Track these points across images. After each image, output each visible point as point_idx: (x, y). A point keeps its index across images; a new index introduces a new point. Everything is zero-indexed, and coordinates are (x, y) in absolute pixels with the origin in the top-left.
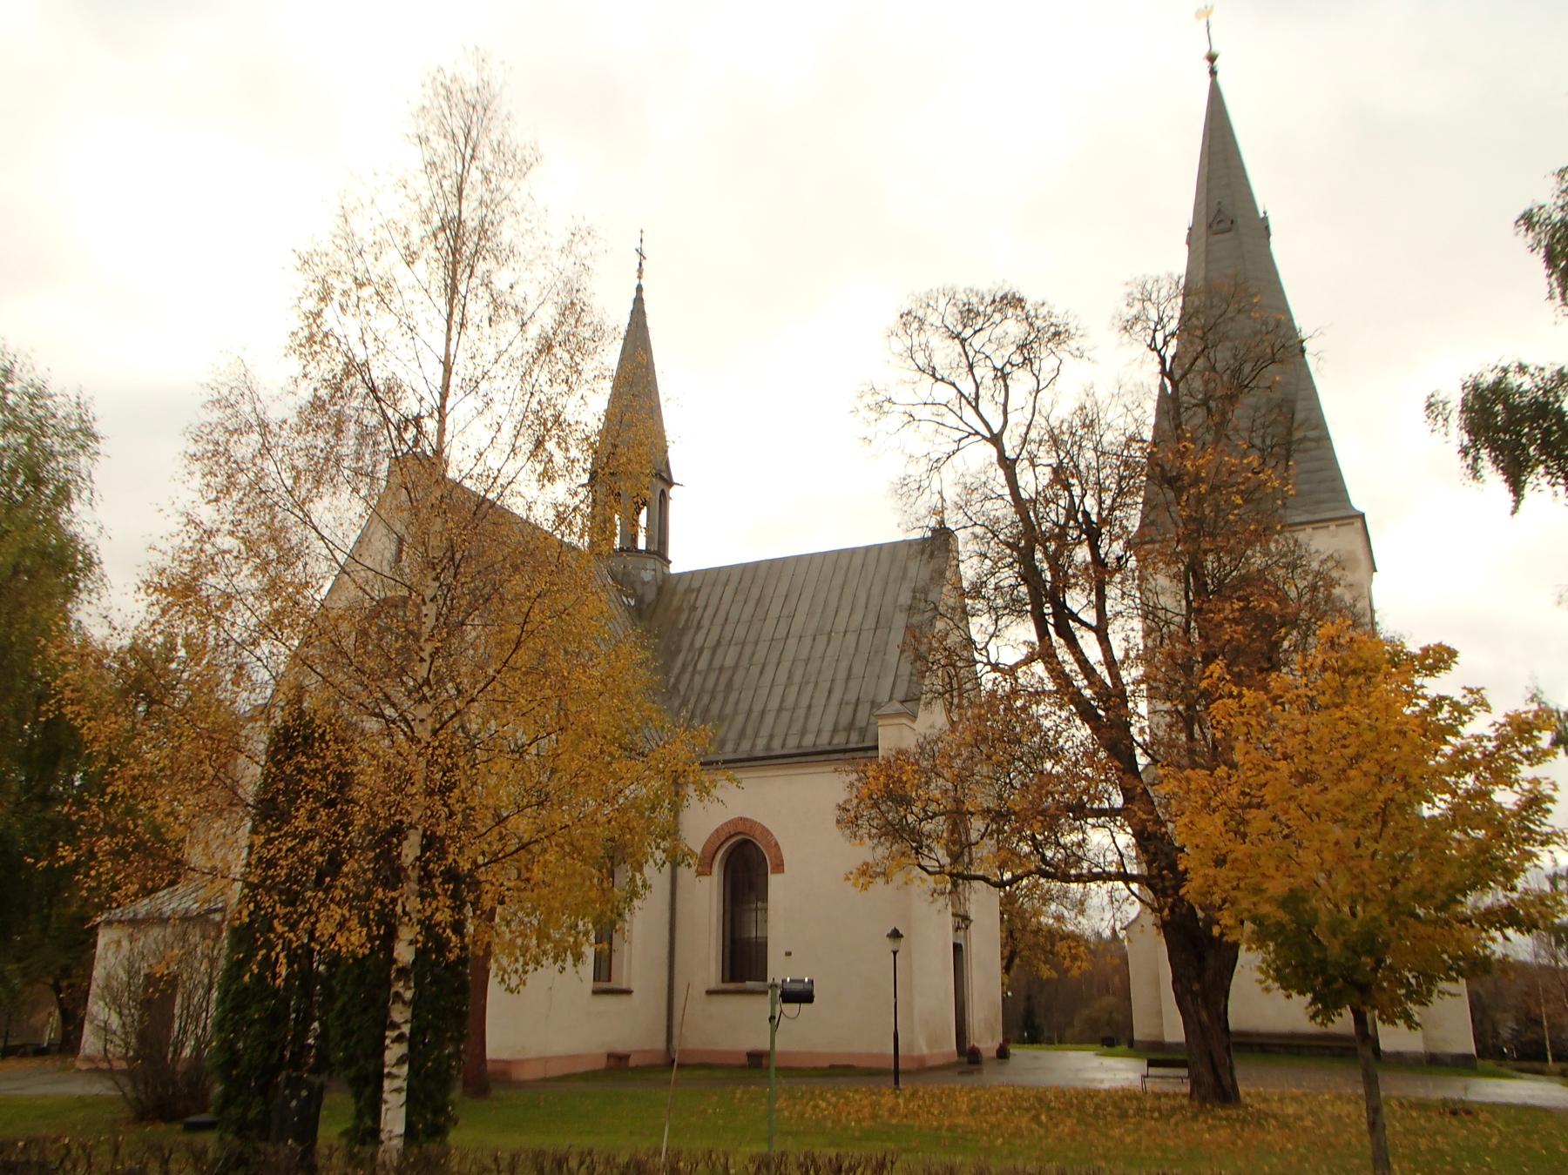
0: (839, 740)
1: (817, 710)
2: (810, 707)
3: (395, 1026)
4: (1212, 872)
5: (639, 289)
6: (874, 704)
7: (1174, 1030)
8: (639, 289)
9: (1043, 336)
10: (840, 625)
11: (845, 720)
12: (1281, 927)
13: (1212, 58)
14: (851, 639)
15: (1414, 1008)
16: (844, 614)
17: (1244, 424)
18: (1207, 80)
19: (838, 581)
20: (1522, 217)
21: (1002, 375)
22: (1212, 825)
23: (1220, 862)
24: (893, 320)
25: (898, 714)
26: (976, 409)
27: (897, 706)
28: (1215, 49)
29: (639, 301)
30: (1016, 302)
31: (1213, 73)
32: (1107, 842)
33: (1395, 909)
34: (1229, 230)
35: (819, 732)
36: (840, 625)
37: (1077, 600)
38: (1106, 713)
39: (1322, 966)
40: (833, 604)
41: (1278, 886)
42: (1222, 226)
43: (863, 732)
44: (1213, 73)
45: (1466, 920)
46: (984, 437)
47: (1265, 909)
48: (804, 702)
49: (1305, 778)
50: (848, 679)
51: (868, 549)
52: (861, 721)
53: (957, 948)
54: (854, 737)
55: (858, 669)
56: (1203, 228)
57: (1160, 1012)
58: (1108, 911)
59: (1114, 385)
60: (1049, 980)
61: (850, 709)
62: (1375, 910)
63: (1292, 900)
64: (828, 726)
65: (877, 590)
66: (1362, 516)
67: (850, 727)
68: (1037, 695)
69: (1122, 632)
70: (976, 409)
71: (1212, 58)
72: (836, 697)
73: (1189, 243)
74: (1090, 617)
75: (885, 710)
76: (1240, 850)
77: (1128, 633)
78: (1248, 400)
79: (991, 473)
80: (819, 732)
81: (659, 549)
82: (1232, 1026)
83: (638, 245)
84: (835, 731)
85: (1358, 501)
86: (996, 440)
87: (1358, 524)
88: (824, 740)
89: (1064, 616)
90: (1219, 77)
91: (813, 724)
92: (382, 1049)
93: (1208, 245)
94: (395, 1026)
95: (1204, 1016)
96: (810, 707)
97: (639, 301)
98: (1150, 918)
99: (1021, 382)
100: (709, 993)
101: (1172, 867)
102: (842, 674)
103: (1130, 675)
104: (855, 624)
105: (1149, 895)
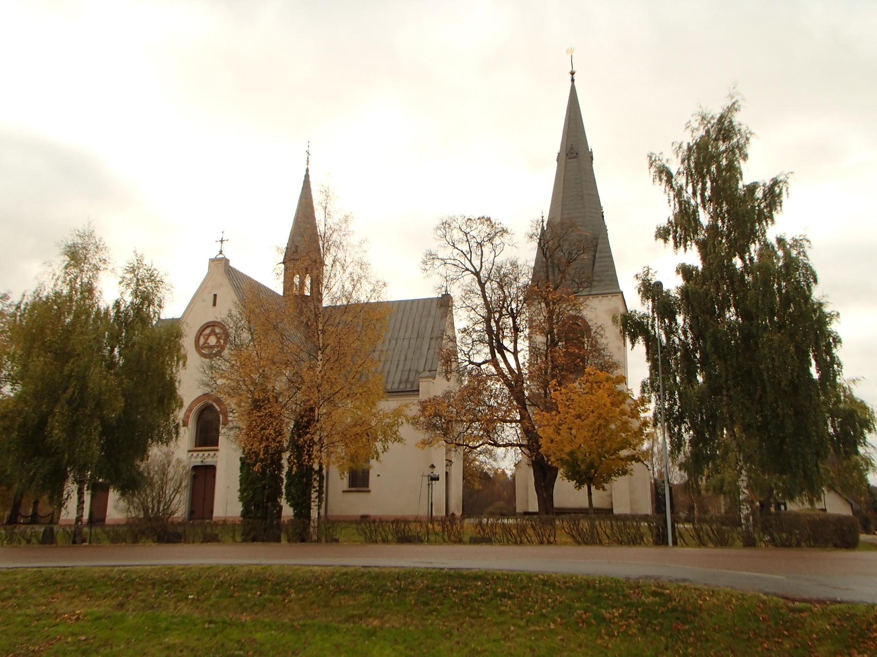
0: (402, 386)
1: (392, 373)
2: (389, 372)
3: (314, 487)
4: (549, 444)
5: (307, 170)
6: (417, 372)
7: (534, 507)
8: (307, 170)
9: (496, 232)
10: (401, 335)
11: (404, 378)
12: (567, 460)
13: (572, 73)
14: (406, 342)
15: (605, 485)
16: (403, 330)
17: (573, 272)
18: (570, 84)
19: (400, 315)
20: (656, 236)
21: (480, 245)
22: (550, 431)
23: (552, 441)
24: (438, 222)
25: (428, 377)
26: (470, 261)
27: (427, 373)
28: (574, 69)
29: (307, 176)
30: (489, 219)
31: (573, 80)
32: (510, 432)
33: (600, 456)
34: (575, 158)
35: (393, 383)
36: (401, 335)
37: (507, 343)
38: (515, 383)
39: (579, 472)
40: (398, 326)
41: (567, 449)
42: (572, 155)
43: (412, 383)
44: (573, 80)
45: (622, 459)
46: (472, 273)
47: (564, 456)
48: (386, 369)
49: (579, 416)
50: (406, 359)
51: (413, 301)
52: (412, 379)
53: (447, 473)
54: (409, 386)
55: (410, 356)
56: (564, 156)
57: (527, 501)
58: (506, 461)
59: (522, 253)
60: (478, 490)
61: (407, 373)
62: (593, 456)
63: (571, 454)
64: (397, 381)
65: (417, 320)
66: (622, 293)
67: (407, 381)
68: (489, 376)
69: (521, 353)
70: (470, 261)
71: (572, 73)
72: (400, 367)
73: (558, 160)
74: (511, 347)
75: (422, 375)
76: (558, 438)
77: (524, 356)
78: (573, 265)
79: (474, 284)
80: (393, 383)
81: (317, 295)
82: (556, 505)
83: (307, 149)
84: (400, 383)
85: (621, 289)
86: (477, 274)
87: (620, 296)
88: (395, 387)
89: (501, 349)
90: (576, 83)
91: (390, 380)
92: (310, 494)
93: (566, 163)
94: (314, 487)
95: (545, 495)
96: (389, 372)
97: (307, 176)
98: (526, 460)
99: (487, 248)
100: (344, 492)
101: (537, 442)
102: (403, 357)
103: (525, 371)
104: (408, 334)
105: (527, 451)
